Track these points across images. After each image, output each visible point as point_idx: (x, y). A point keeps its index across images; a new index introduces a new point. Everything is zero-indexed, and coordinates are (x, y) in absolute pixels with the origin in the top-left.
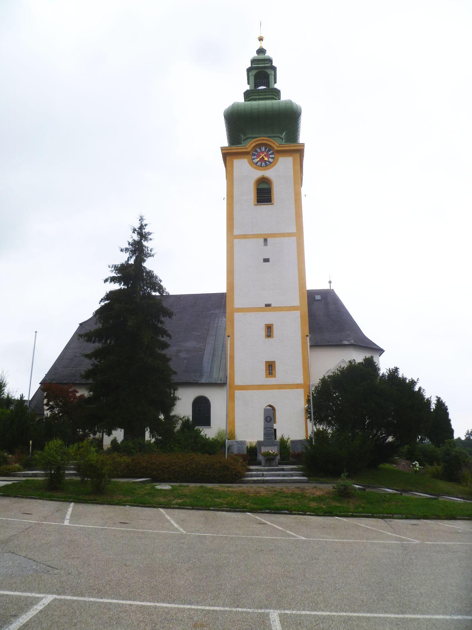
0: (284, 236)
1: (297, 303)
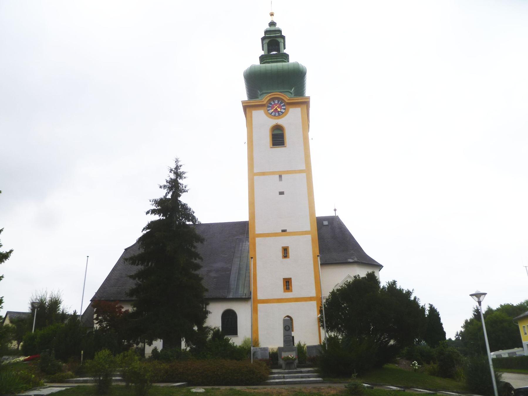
0: (296, 173)
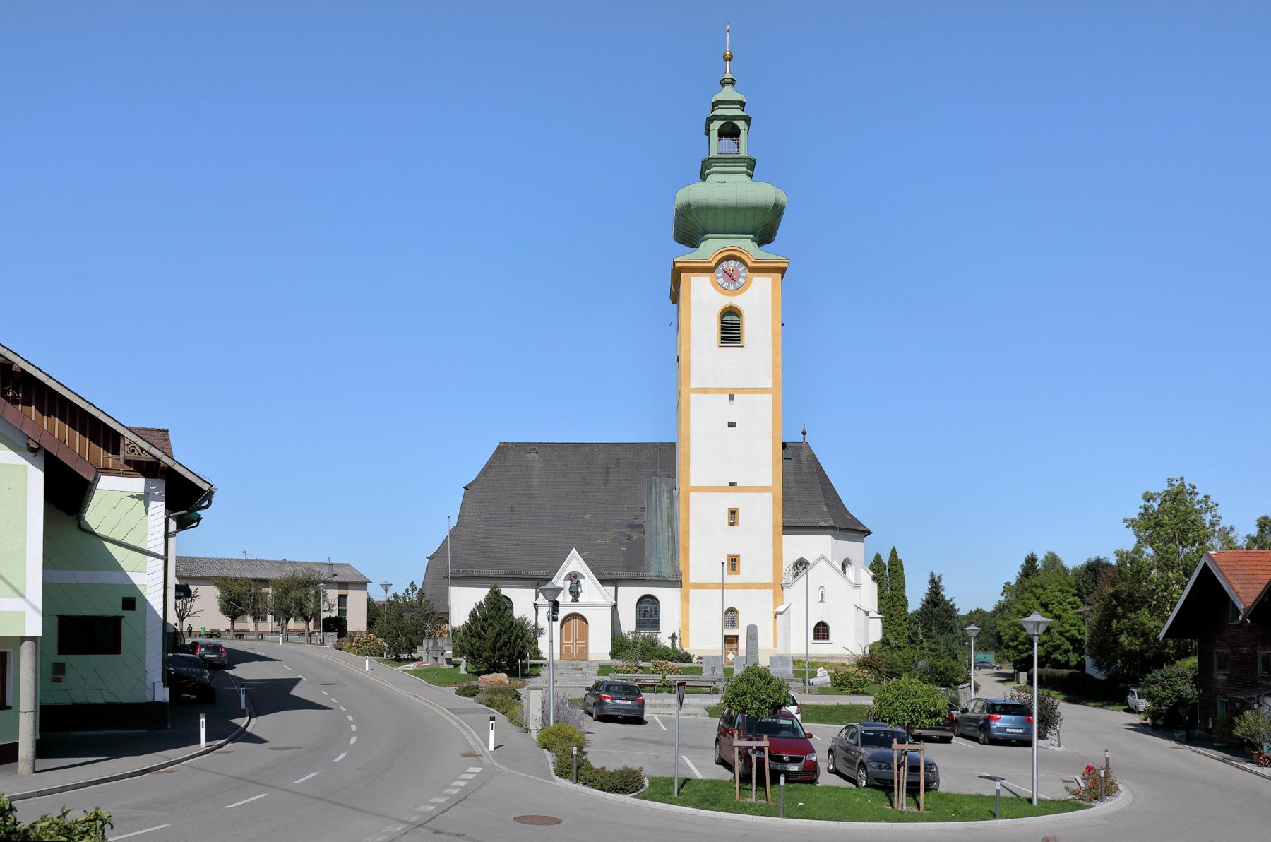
1: (768, 482)
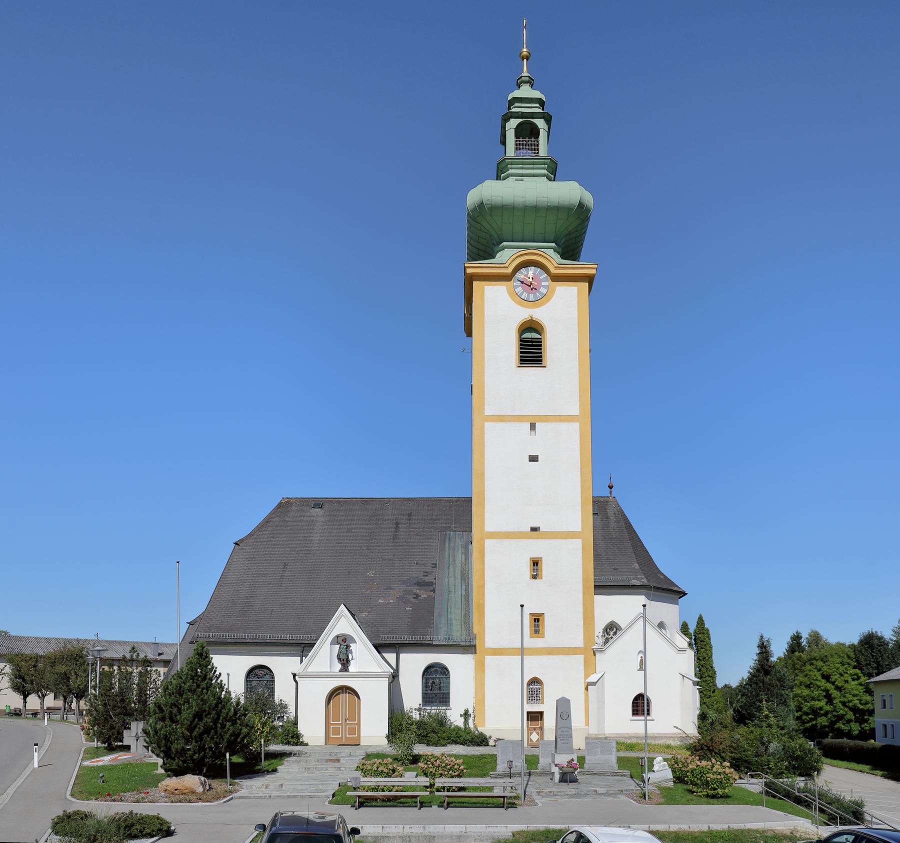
0: (561, 421)
1: (577, 527)
